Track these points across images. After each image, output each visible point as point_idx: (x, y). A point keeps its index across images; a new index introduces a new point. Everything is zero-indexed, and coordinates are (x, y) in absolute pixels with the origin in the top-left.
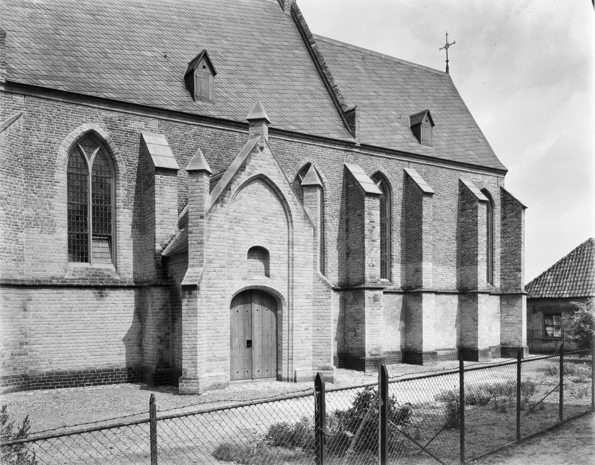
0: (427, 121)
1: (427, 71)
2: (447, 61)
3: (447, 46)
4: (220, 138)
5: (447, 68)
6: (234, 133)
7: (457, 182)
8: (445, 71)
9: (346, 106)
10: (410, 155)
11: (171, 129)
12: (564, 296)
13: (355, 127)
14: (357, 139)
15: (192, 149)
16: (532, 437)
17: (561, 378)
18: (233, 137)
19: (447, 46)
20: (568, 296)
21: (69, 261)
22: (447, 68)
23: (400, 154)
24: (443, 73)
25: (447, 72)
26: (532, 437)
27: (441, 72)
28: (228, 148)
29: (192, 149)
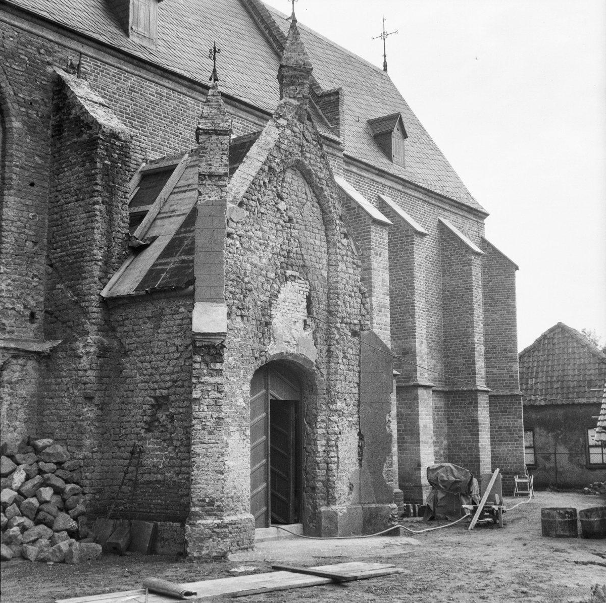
0: (398, 130)
1: (365, 64)
2: (385, 56)
3: (384, 36)
4: (167, 103)
5: (385, 65)
6: (187, 99)
7: (435, 222)
8: (382, 69)
9: (319, 87)
10: (387, 176)
11: (98, 73)
12: (537, 403)
13: (339, 119)
14: (342, 138)
15: (127, 113)
16: (41, 413)
17: (79, 370)
18: (186, 105)
19: (384, 36)
20: (543, 403)
21: (543, 510)
22: (385, 65)
23: (374, 171)
24: (381, 70)
25: (385, 70)
26: (41, 413)
27: (379, 69)
28: (178, 122)
29: (127, 113)
